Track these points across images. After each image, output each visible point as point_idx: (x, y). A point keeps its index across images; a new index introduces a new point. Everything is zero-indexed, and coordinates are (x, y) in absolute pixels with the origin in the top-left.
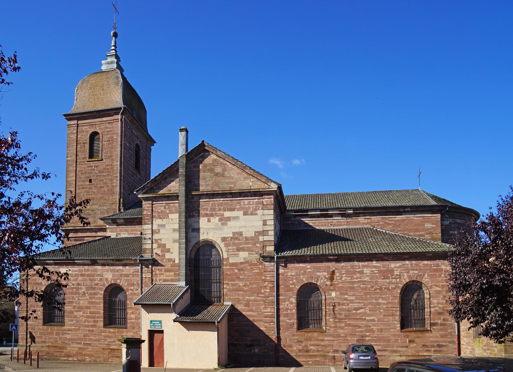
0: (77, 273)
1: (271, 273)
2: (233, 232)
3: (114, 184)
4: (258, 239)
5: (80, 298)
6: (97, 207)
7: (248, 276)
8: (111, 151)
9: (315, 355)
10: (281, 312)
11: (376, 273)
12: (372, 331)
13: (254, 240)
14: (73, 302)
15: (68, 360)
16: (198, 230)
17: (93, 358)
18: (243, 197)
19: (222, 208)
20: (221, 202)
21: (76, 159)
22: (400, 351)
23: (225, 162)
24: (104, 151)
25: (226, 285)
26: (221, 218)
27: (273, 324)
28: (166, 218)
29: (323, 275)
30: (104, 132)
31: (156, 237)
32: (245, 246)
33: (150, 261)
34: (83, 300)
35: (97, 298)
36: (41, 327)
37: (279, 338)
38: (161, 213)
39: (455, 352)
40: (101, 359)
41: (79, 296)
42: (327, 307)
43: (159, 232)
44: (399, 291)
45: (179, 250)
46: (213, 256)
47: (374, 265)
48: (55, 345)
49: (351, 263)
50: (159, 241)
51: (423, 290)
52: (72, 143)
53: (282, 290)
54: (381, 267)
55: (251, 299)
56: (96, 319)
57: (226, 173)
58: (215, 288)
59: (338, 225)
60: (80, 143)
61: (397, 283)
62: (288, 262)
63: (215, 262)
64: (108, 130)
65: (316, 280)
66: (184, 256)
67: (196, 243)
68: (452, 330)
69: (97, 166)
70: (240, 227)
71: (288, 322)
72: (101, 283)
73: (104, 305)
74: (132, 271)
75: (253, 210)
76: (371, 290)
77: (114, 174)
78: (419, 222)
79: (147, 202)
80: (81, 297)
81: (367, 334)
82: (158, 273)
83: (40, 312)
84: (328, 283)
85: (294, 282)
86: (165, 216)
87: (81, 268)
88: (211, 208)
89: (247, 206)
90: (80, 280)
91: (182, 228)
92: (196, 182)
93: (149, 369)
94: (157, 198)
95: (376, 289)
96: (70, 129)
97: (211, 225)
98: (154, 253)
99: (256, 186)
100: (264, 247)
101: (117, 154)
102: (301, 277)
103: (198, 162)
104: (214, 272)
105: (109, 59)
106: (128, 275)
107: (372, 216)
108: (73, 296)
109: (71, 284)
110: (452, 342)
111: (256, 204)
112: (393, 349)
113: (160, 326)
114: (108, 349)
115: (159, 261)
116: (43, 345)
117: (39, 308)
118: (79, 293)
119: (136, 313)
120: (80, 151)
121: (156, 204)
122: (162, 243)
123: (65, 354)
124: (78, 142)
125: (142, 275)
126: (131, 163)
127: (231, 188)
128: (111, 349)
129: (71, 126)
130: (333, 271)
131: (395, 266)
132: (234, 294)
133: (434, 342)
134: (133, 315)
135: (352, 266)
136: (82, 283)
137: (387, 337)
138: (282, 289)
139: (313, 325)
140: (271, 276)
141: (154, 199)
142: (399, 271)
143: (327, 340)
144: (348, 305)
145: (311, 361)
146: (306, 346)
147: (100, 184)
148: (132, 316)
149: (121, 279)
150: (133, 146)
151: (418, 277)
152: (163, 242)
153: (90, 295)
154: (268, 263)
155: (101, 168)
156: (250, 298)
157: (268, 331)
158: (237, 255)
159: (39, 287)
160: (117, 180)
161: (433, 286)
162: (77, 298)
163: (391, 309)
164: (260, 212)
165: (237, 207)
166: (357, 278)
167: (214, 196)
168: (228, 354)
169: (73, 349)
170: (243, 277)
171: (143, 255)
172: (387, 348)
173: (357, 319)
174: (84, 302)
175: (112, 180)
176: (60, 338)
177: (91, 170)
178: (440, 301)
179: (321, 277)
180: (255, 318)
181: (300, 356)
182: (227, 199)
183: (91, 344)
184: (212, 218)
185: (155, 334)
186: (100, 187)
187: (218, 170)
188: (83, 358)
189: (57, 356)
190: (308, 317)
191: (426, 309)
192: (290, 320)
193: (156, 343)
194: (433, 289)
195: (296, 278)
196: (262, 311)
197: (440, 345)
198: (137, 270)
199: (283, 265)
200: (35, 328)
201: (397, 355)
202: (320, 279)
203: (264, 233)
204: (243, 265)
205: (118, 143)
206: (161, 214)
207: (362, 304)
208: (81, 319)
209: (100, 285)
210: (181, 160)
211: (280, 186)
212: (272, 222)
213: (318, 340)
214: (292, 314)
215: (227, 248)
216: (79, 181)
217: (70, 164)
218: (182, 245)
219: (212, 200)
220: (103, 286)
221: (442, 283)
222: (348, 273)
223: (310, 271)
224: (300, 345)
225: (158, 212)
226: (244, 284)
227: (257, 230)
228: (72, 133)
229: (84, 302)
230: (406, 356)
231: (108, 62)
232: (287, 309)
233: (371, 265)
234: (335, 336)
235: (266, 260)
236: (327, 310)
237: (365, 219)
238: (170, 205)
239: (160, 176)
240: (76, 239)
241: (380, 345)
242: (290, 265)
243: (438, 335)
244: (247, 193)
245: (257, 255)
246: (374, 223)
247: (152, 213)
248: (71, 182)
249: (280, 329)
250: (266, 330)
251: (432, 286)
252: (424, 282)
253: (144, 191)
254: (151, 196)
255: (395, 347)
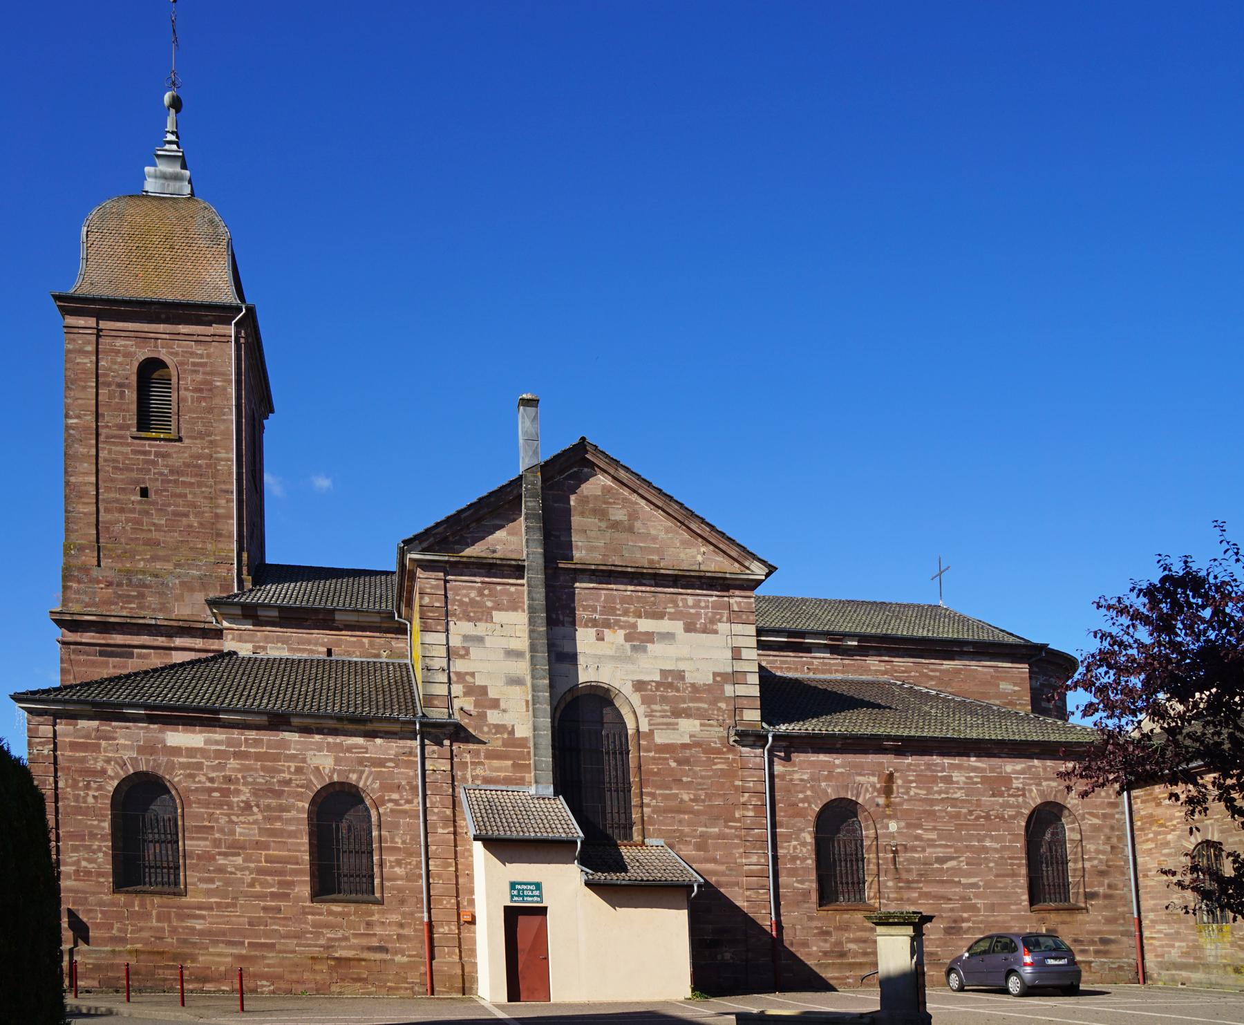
0: (223, 748)
2: (661, 670)
3: (220, 511)
4: (723, 691)
5: (234, 818)
6: (169, 566)
7: (702, 777)
8: (207, 418)
9: (861, 964)
10: (781, 866)
11: (977, 783)
12: (974, 908)
13: (712, 691)
15: (202, 991)
16: (572, 658)
18: (682, 588)
19: (632, 608)
20: (629, 593)
21: (97, 426)
23: (634, 497)
25: (649, 798)
26: (629, 633)
28: (486, 621)
29: (868, 782)
30: (182, 364)
31: (459, 666)
32: (691, 705)
34: (244, 823)
39: (1132, 954)
40: (307, 986)
42: (881, 855)
43: (466, 654)
44: (1023, 824)
46: (605, 725)
47: (972, 766)
49: (926, 758)
50: (468, 678)
51: (1063, 824)
52: (80, 379)
53: (782, 814)
54: (985, 769)
59: (824, 672)
61: (1019, 806)
62: (792, 749)
64: (197, 360)
65: (855, 792)
66: (546, 722)
68: (1126, 909)
69: (165, 455)
70: (678, 659)
72: (298, 780)
73: (310, 840)
74: (393, 752)
75: (708, 621)
76: (969, 820)
77: (220, 482)
78: (989, 677)
79: (433, 574)
80: (238, 816)
81: (965, 915)
82: (468, 760)
83: (101, 855)
84: (881, 801)
85: (806, 797)
86: (483, 615)
87: (235, 734)
88: (605, 607)
89: (692, 611)
90: (234, 770)
91: (540, 648)
93: (509, 1006)
94: (460, 566)
95: (978, 818)
97: (604, 648)
99: (713, 566)
100: (736, 710)
101: (227, 433)
102: (823, 784)
103: (565, 488)
104: (609, 763)
106: (381, 763)
107: (894, 657)
109: (203, 779)
110: (1126, 933)
111: (713, 608)
113: (537, 896)
114: (328, 958)
115: (470, 730)
116: (117, 949)
117: (97, 843)
118: (230, 806)
119: (410, 864)
120: (108, 404)
121: (457, 582)
122: (477, 684)
124: (101, 380)
127: (651, 561)
129: (76, 330)
130: (891, 775)
131: (1013, 769)
132: (669, 821)
134: (401, 867)
135: (929, 765)
136: (239, 776)
137: (1004, 922)
138: (781, 811)
140: (755, 779)
141: (450, 567)
142: (1022, 780)
144: (924, 850)
148: (397, 870)
149: (362, 772)
151: (1059, 795)
152: (479, 681)
153: (265, 811)
155: (177, 461)
158: (672, 727)
159: (95, 782)
161: (1087, 816)
163: (1009, 861)
166: (940, 793)
167: (610, 576)
169: (217, 959)
170: (689, 779)
173: (943, 882)
174: (248, 829)
175: (211, 498)
176: (174, 930)
177: (146, 462)
178: (1101, 848)
179: (865, 786)
180: (723, 879)
182: (643, 588)
183: (273, 945)
184: (606, 631)
185: (520, 918)
186: (175, 514)
187: (619, 514)
189: (165, 980)
191: (1070, 864)
192: (802, 882)
193: (523, 943)
194: (1086, 821)
195: (812, 786)
198: (407, 750)
199: (782, 754)
200: (86, 899)
202: (863, 791)
203: (735, 677)
204: (688, 751)
206: (470, 609)
207: (953, 850)
208: (239, 876)
209: (298, 786)
210: (530, 477)
214: (806, 869)
215: (649, 707)
216: (108, 489)
219: (604, 586)
220: (307, 787)
221: (1104, 809)
222: (924, 780)
223: (841, 773)
224: (826, 941)
225: (461, 603)
226: (692, 797)
227: (717, 670)
229: (248, 829)
232: (794, 859)
233: (966, 764)
235: (745, 743)
236: (881, 862)
237: (880, 661)
238: (495, 588)
239: (472, 511)
240: (106, 651)
242: (798, 757)
243: (1100, 918)
244: (693, 580)
245: (722, 729)
246: (900, 673)
247: (446, 603)
248: (83, 488)
251: (1084, 814)
252: (1069, 806)
253: (425, 545)
254: (446, 558)
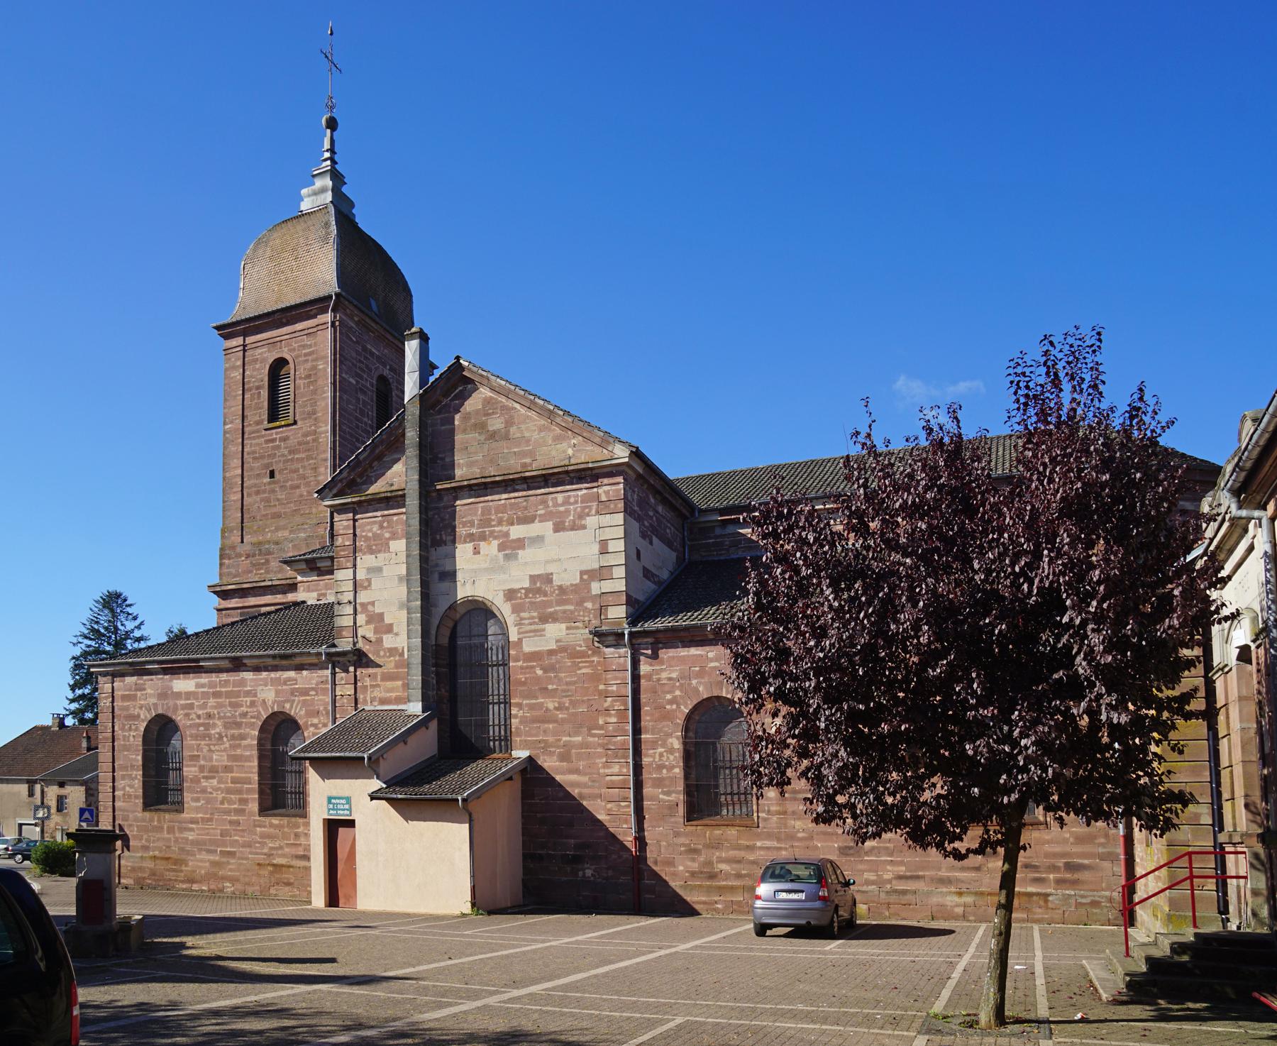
0: (205, 690)
1: (620, 674)
2: (531, 576)
4: (589, 590)
5: (212, 747)
6: (286, 533)
7: (568, 684)
10: (645, 775)
13: (578, 592)
14: (199, 756)
15: (192, 890)
16: (451, 576)
17: (239, 886)
18: (552, 487)
20: (503, 502)
21: (243, 426)
22: (958, 880)
23: (511, 404)
24: (300, 402)
27: (626, 806)
28: (385, 552)
30: (298, 356)
31: (363, 597)
32: (558, 608)
33: (349, 656)
34: (218, 751)
35: (246, 747)
36: (140, 815)
37: (641, 840)
38: (374, 540)
41: (210, 742)
45: (408, 626)
46: (490, 638)
48: (166, 856)
53: (648, 718)
55: (574, 742)
56: (245, 796)
57: (513, 430)
58: (496, 716)
60: (250, 389)
62: (661, 645)
63: (494, 651)
66: (417, 641)
67: (449, 608)
69: (284, 439)
71: (663, 799)
74: (314, 682)
79: (344, 516)
80: (214, 745)
83: (136, 781)
85: (675, 697)
87: (214, 678)
88: (481, 520)
89: (562, 509)
90: (212, 707)
92: (447, 460)
96: (230, 359)
97: (481, 562)
98: (359, 636)
99: (583, 457)
100: (602, 609)
102: (694, 682)
105: (319, 183)
106: (305, 692)
108: (198, 742)
110: (1111, 857)
111: (582, 502)
112: (940, 873)
114: (269, 864)
115: (370, 655)
118: (209, 736)
120: (250, 406)
123: (185, 876)
124: (246, 387)
125: (334, 690)
126: (366, 424)
127: (524, 465)
128: (274, 865)
133: (1055, 855)
136: (216, 712)
139: (730, 808)
140: (620, 684)
143: (761, 848)
145: (720, 902)
146: (709, 863)
147: (292, 480)
150: (370, 382)
153: (232, 740)
154: (612, 650)
155: (292, 442)
156: (573, 739)
157: (614, 822)
160: (326, 468)
162: (207, 748)
164: (591, 521)
165: (539, 512)
168: (523, 880)
169: (200, 864)
170: (555, 687)
171: (336, 642)
172: (921, 871)
176: (176, 840)
177: (274, 448)
180: (585, 791)
181: (693, 888)
182: (516, 494)
184: (482, 543)
187: (496, 423)
188: (220, 886)
189: (170, 880)
190: (717, 786)
192: (668, 793)
195: (682, 685)
196: (602, 771)
197: (1073, 866)
199: (649, 652)
200: (128, 816)
201: (950, 892)
203: (602, 573)
204: (554, 657)
205: (327, 379)
206: (373, 543)
208: (215, 795)
209: (252, 717)
211: (634, 450)
212: (620, 545)
213: (739, 848)
214: (673, 779)
215: (518, 616)
217: (231, 438)
218: (415, 613)
219: (482, 499)
220: (257, 717)
224: (693, 860)
225: (367, 539)
226: (557, 705)
227: (584, 568)
228: (234, 368)
230: (976, 894)
231: (315, 190)
234: (783, 836)
235: (607, 643)
241: (901, 863)
244: (561, 476)
247: (355, 541)
248: (234, 480)
249: (644, 818)
250: (609, 821)
253: (335, 491)
254: (349, 500)
255: (943, 870)
